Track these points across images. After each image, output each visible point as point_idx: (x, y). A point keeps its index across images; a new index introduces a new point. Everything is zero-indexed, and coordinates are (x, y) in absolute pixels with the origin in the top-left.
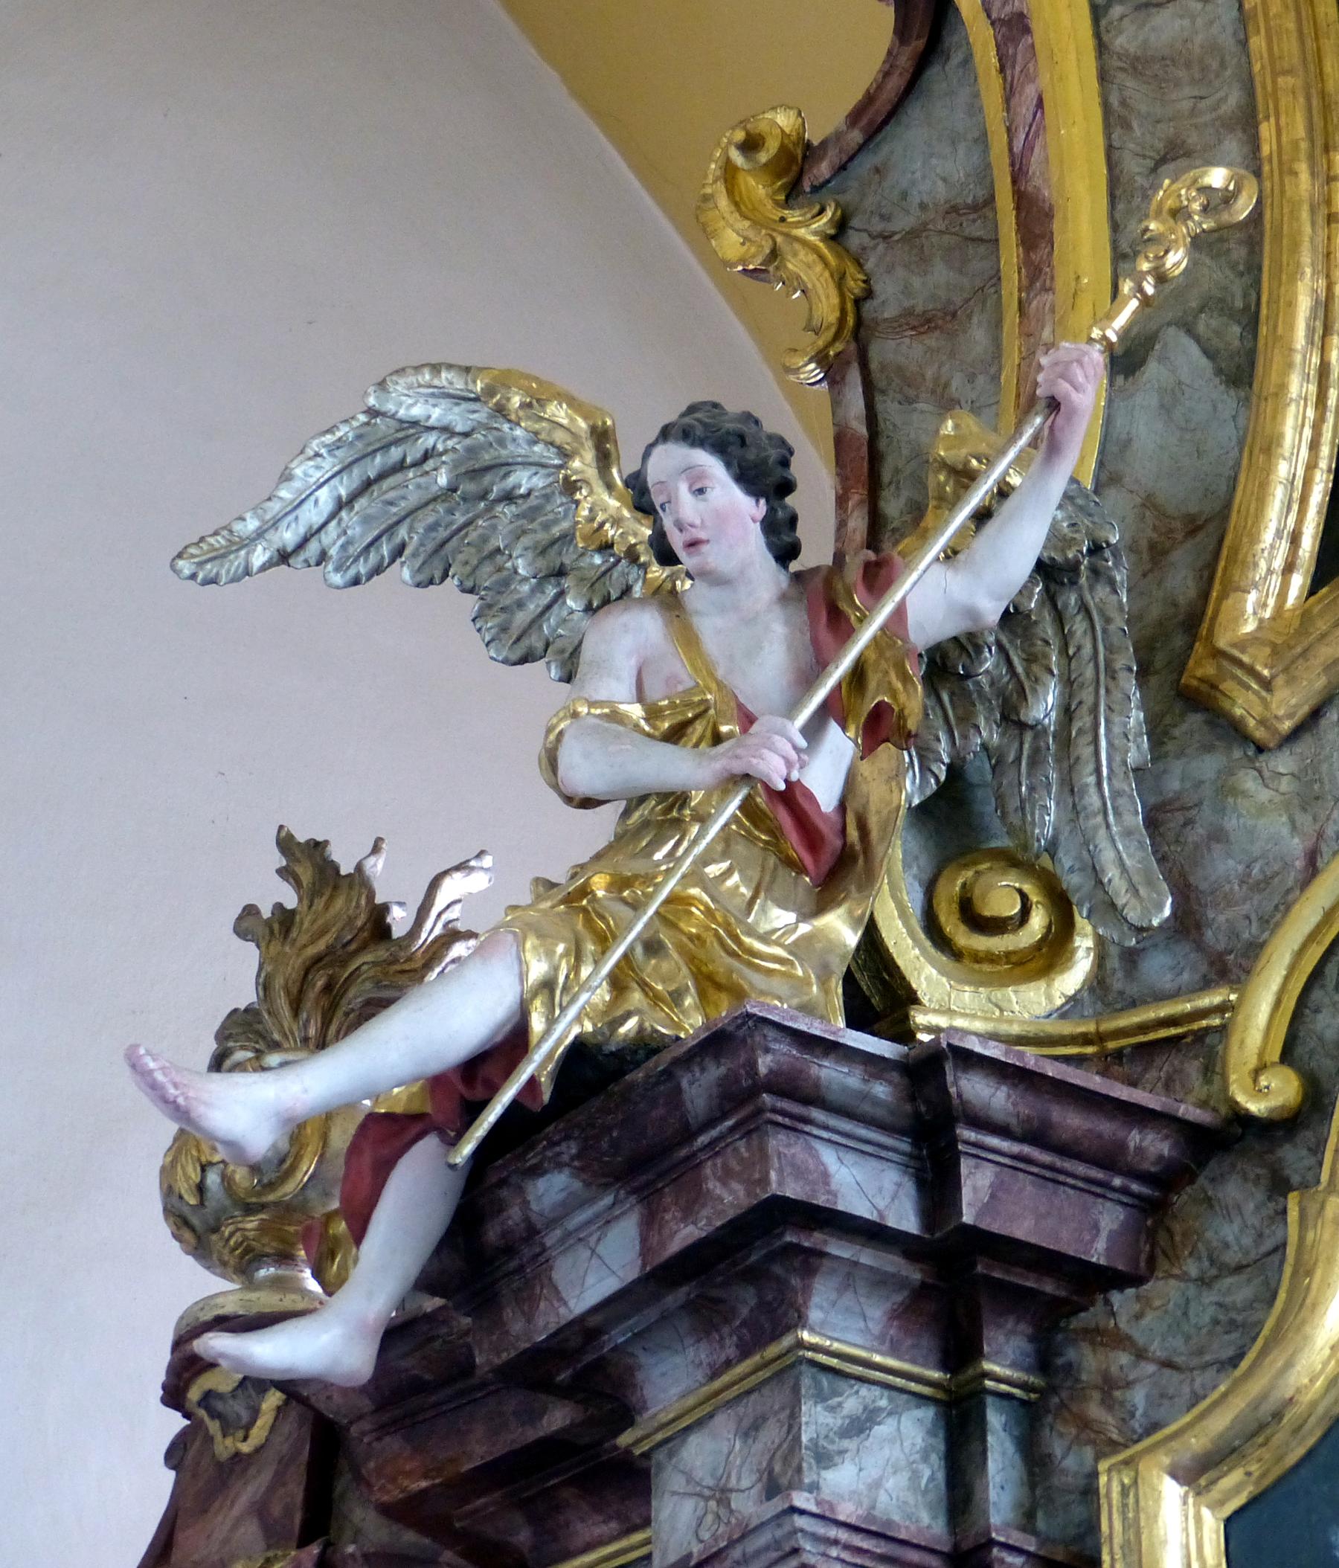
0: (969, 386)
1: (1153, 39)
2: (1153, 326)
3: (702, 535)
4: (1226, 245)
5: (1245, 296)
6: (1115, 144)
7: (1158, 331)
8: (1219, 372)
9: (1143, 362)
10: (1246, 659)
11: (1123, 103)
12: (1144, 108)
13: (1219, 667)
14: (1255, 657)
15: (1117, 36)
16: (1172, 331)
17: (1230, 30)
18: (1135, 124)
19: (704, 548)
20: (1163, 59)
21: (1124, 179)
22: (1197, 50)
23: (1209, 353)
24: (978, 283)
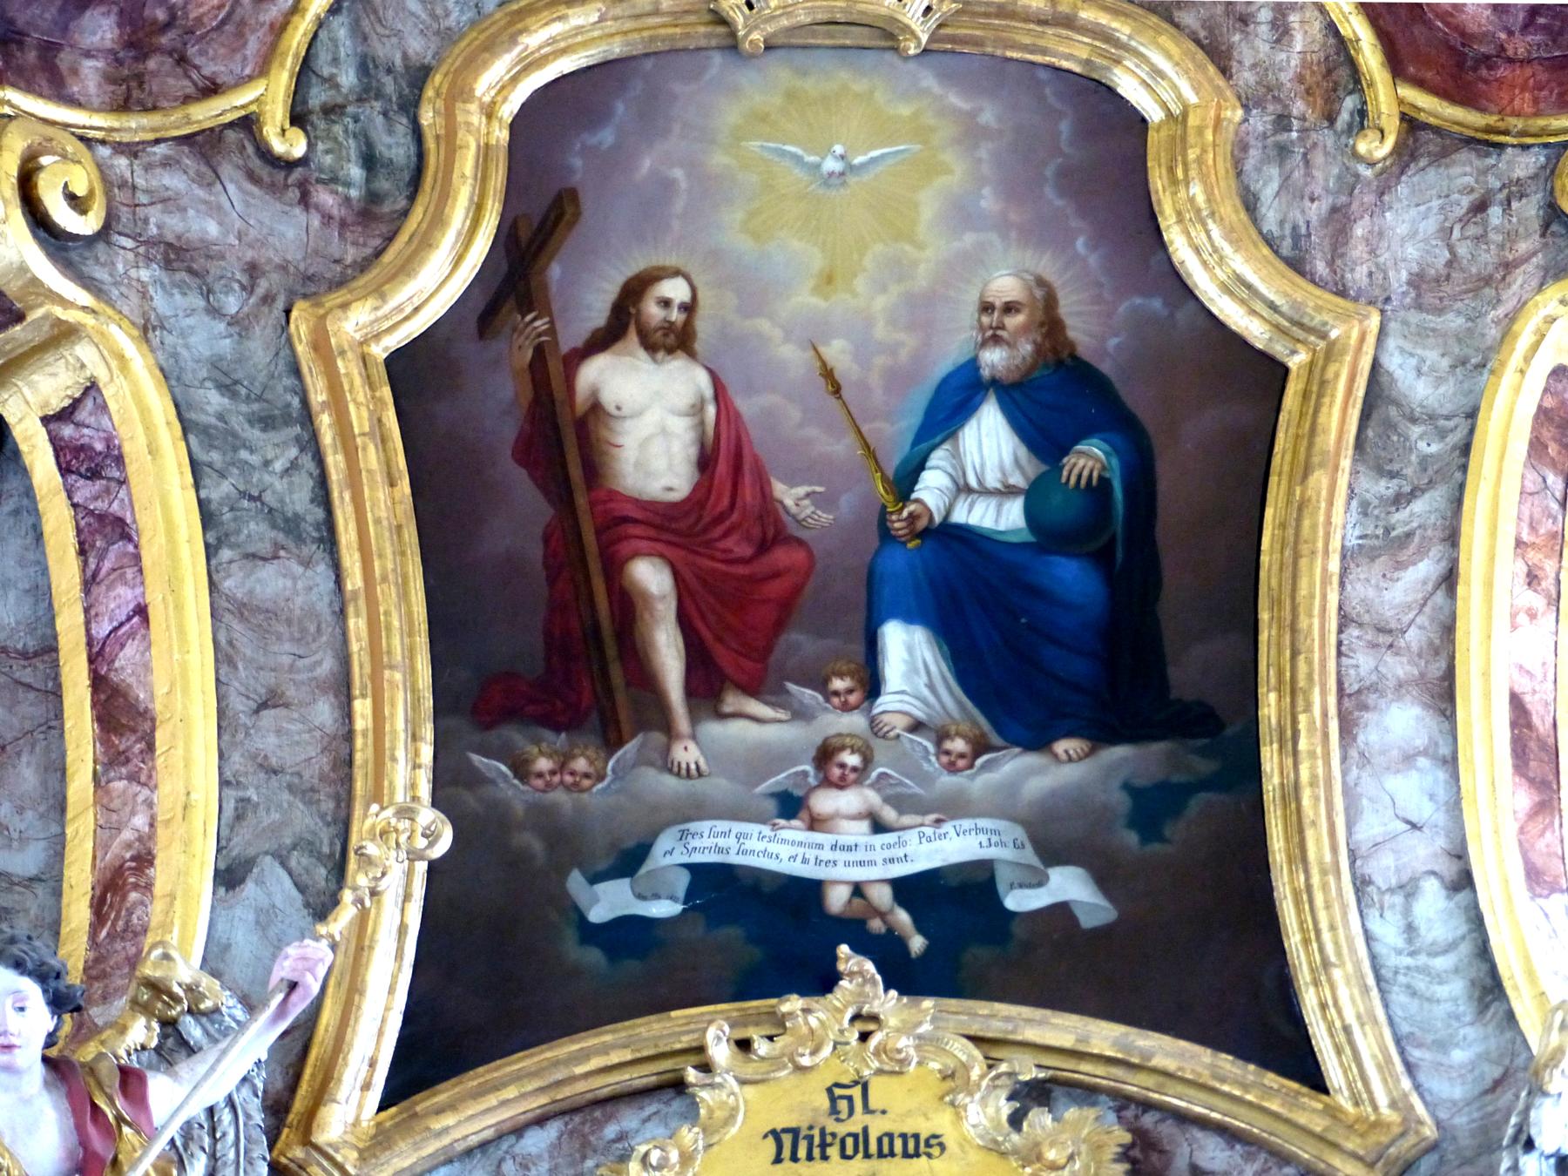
0: (17, 818)
1: (258, 589)
2: (251, 851)
3: (14, 1041)
4: (316, 796)
5: (332, 844)
6: (223, 679)
7: (257, 856)
8: (307, 905)
9: (242, 881)
10: (339, 1158)
11: (230, 643)
12: (248, 652)
13: (308, 1153)
14: (345, 1157)
15: (225, 578)
16: (268, 859)
17: (326, 600)
18: (240, 666)
19: (16, 1051)
20: (267, 611)
21: (230, 713)
22: (298, 612)
23: (301, 888)
24: (28, 726)
